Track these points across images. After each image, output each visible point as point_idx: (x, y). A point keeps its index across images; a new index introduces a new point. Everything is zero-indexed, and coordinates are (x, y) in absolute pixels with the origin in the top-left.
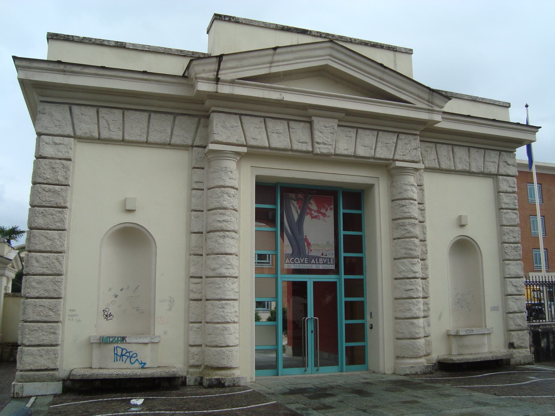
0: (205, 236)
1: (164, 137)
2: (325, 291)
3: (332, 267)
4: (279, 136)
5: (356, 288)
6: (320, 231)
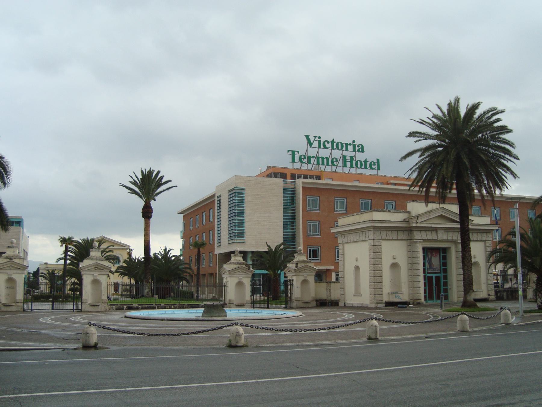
0: (412, 265)
1: (401, 238)
2: (438, 278)
3: (439, 271)
4: (430, 236)
5: (445, 277)
6: (436, 261)
